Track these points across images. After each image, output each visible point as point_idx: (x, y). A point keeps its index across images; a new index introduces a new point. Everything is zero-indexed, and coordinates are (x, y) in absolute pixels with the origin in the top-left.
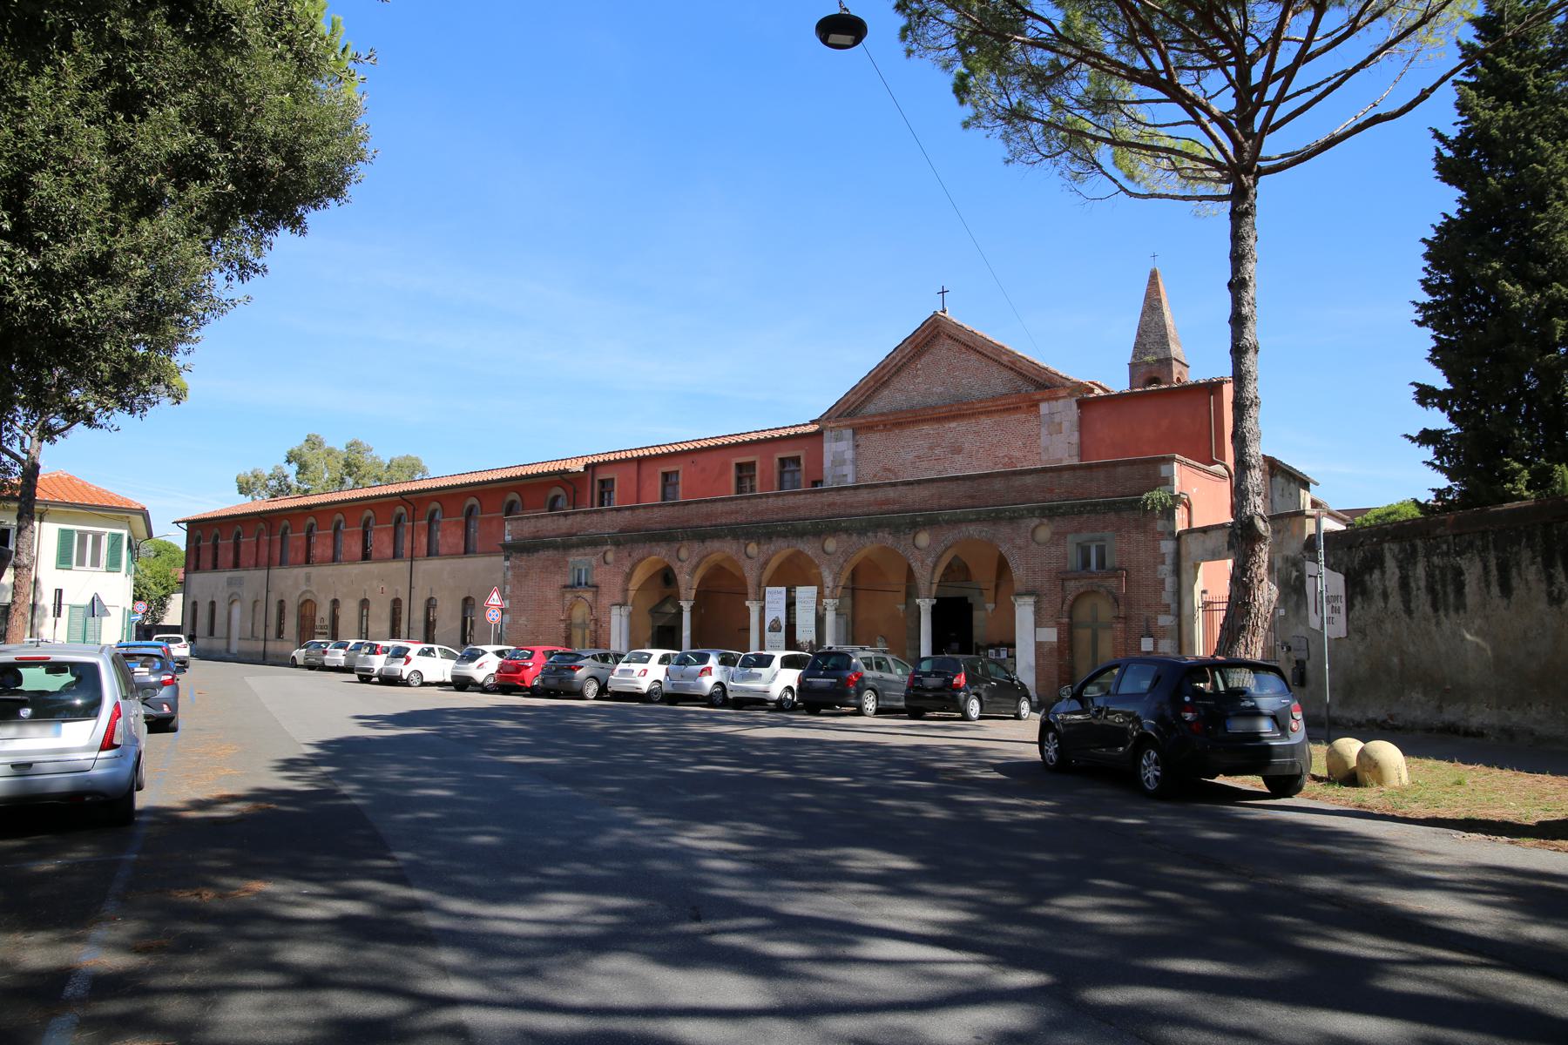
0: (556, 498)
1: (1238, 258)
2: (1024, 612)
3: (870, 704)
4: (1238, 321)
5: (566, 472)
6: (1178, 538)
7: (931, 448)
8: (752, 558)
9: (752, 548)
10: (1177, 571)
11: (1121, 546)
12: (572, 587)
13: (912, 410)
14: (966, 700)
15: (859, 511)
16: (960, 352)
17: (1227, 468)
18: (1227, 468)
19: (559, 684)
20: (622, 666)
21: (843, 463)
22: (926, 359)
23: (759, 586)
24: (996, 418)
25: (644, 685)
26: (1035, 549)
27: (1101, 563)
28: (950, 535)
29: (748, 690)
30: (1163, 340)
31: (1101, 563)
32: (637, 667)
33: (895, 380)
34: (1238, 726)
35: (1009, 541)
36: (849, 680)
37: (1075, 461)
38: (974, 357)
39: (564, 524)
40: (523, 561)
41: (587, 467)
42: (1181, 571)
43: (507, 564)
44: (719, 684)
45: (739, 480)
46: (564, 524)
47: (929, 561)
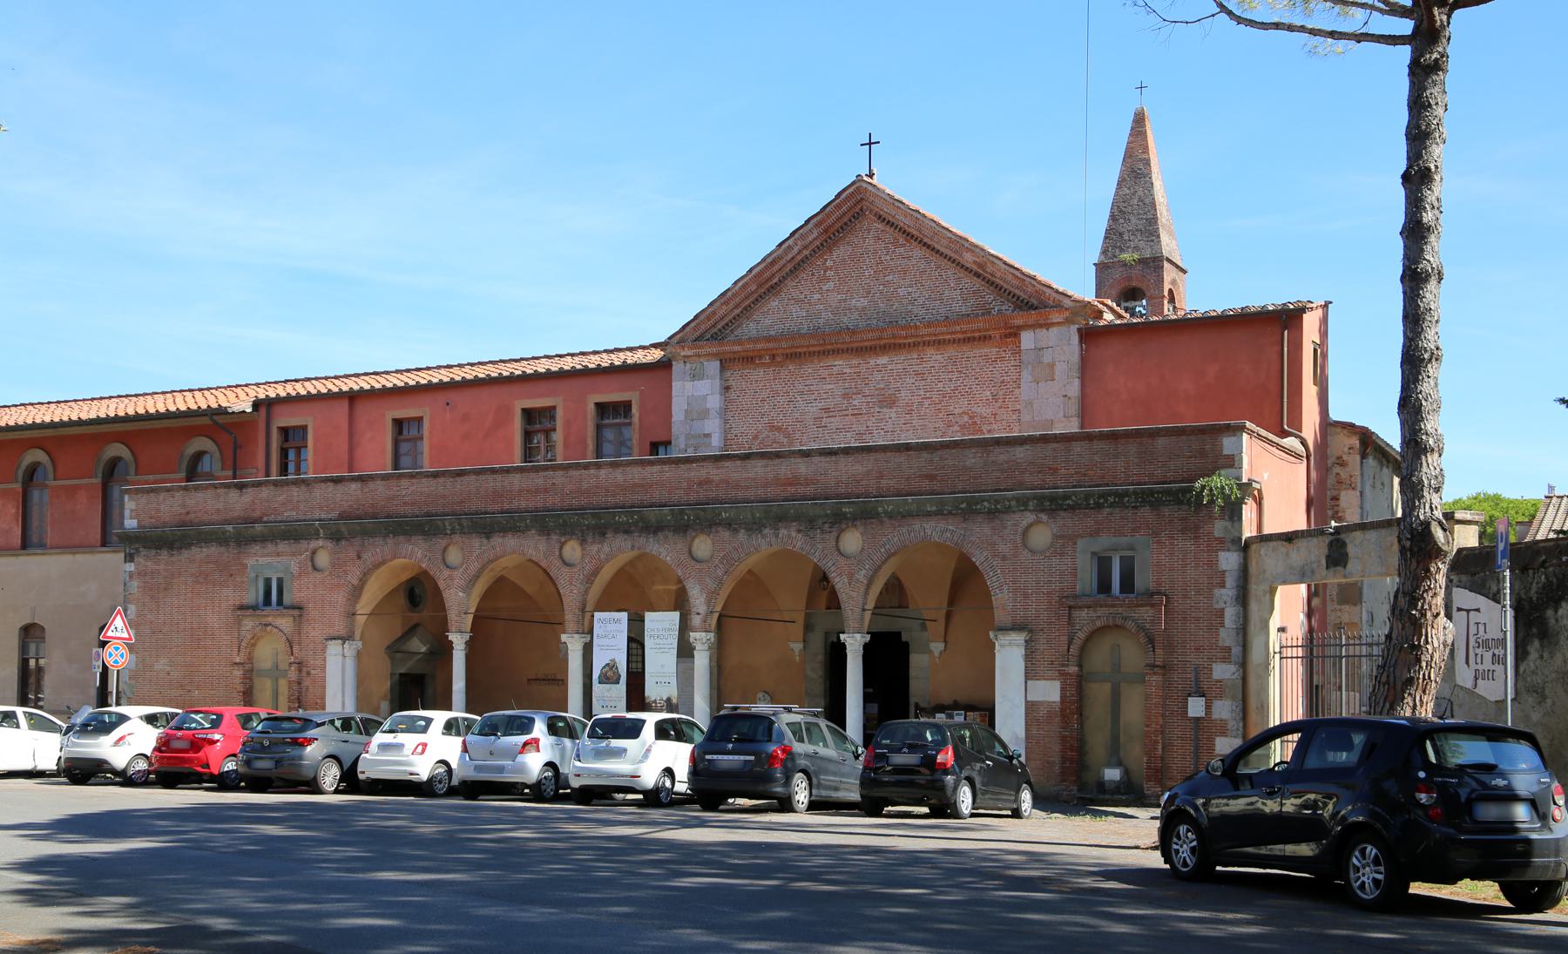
0: (199, 456)
1: (1419, 136)
2: (1009, 657)
3: (802, 796)
4: (1416, 232)
5: (222, 411)
6: (1245, 547)
7: (846, 396)
8: (575, 563)
9: (572, 550)
10: (1243, 598)
11: (1158, 559)
12: (255, 608)
13: (816, 333)
14: (955, 789)
15: (750, 494)
16: (895, 243)
17: (1304, 443)
18: (1304, 443)
19: (272, 768)
20: (379, 738)
21: (704, 414)
22: (841, 252)
23: (583, 610)
24: (951, 351)
25: (423, 769)
26: (1029, 559)
27: (1128, 584)
28: (894, 536)
29: (599, 774)
30: (1150, 229)
31: (1128, 584)
32: (409, 740)
33: (790, 283)
34: (1489, 812)
35: (981, 542)
36: (772, 758)
37: (1073, 427)
38: (918, 252)
39: (237, 503)
40: (161, 563)
41: (257, 404)
42: (1248, 596)
43: (131, 567)
44: (550, 765)
45: (528, 435)
46: (237, 503)
47: (862, 575)
